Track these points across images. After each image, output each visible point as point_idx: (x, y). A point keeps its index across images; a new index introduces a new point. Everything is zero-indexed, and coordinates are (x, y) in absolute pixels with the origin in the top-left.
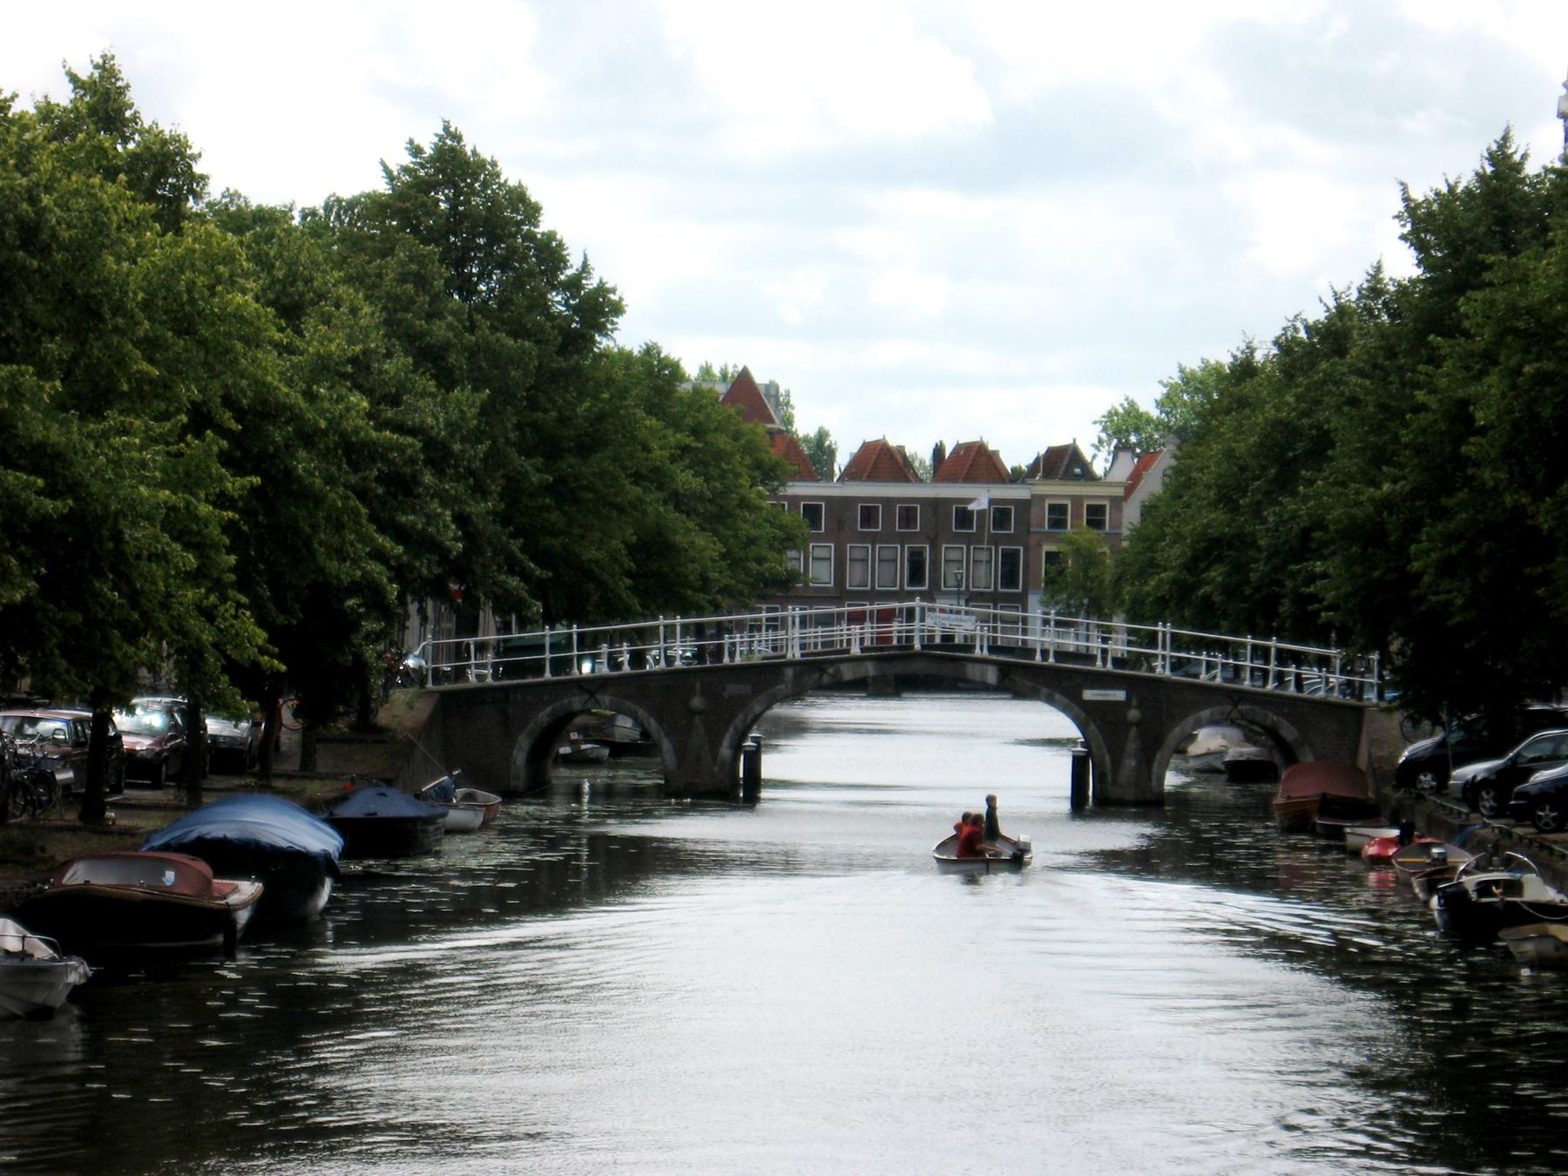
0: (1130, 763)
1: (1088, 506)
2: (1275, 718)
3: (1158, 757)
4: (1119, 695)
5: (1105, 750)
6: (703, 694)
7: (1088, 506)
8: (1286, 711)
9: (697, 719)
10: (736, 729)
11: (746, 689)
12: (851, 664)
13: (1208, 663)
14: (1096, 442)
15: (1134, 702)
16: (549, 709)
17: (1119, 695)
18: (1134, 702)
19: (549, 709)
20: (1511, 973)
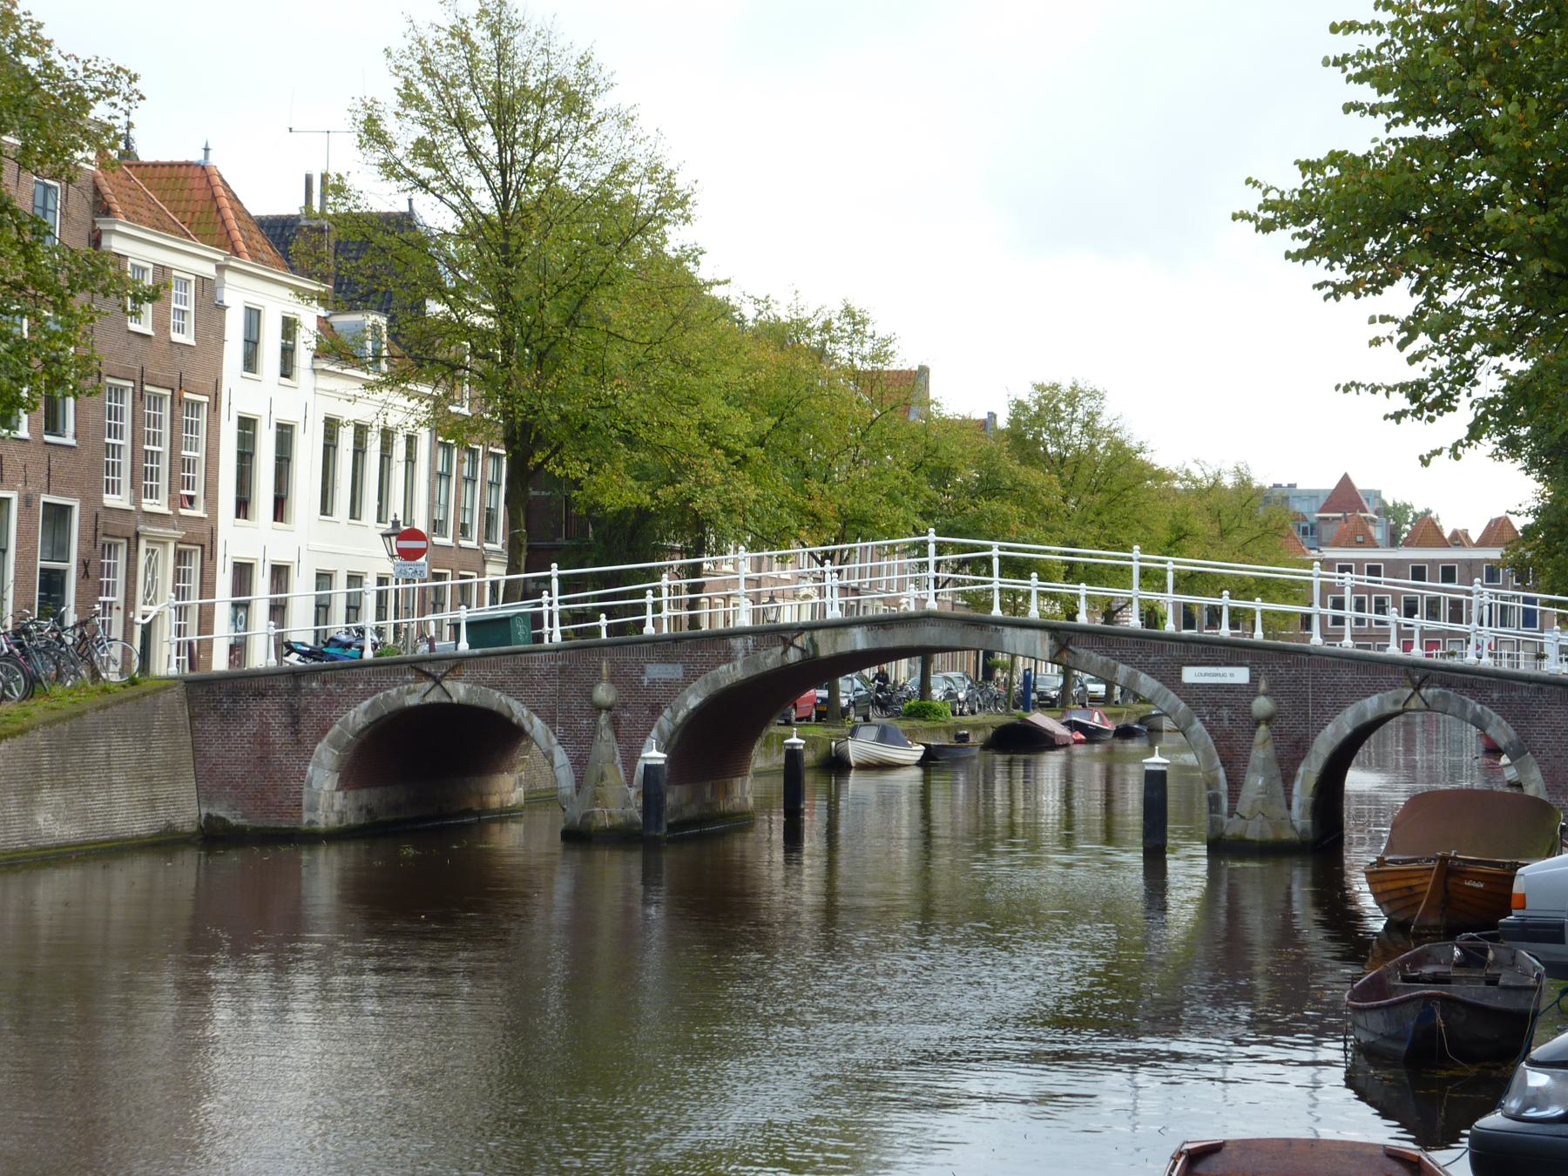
0: (1255, 782)
1: (70, 507)
2: (1478, 707)
3: (1301, 770)
4: (1240, 675)
5: (1218, 762)
6: (612, 680)
7: (70, 507)
8: (1495, 695)
9: (603, 718)
10: (660, 731)
11: (674, 671)
12: (828, 631)
13: (1234, 612)
14: (700, 258)
15: (1263, 686)
16: (367, 703)
17: (1240, 675)
18: (1263, 686)
19: (367, 703)
20: (463, 807)
